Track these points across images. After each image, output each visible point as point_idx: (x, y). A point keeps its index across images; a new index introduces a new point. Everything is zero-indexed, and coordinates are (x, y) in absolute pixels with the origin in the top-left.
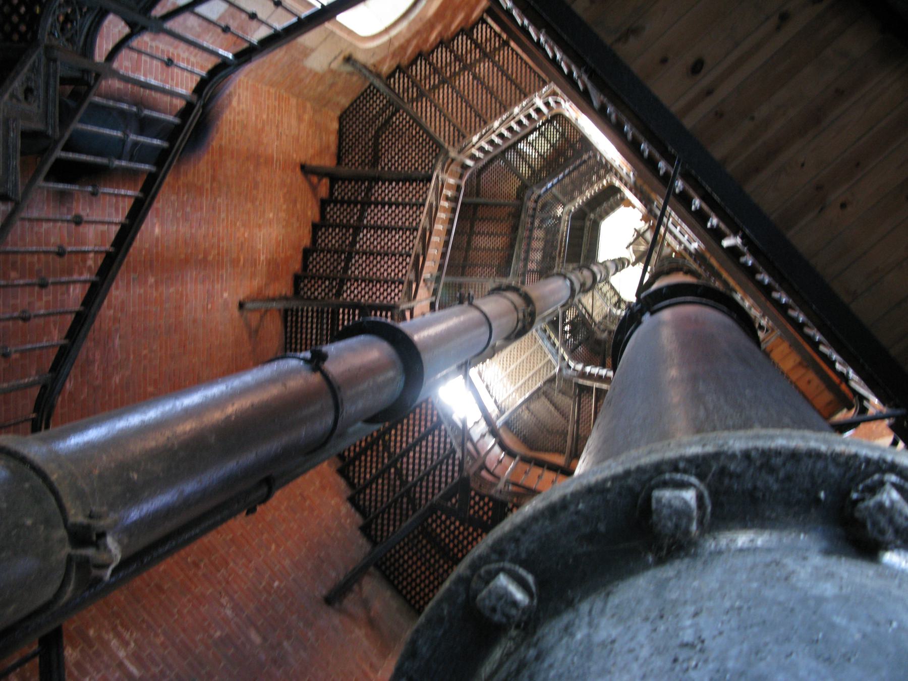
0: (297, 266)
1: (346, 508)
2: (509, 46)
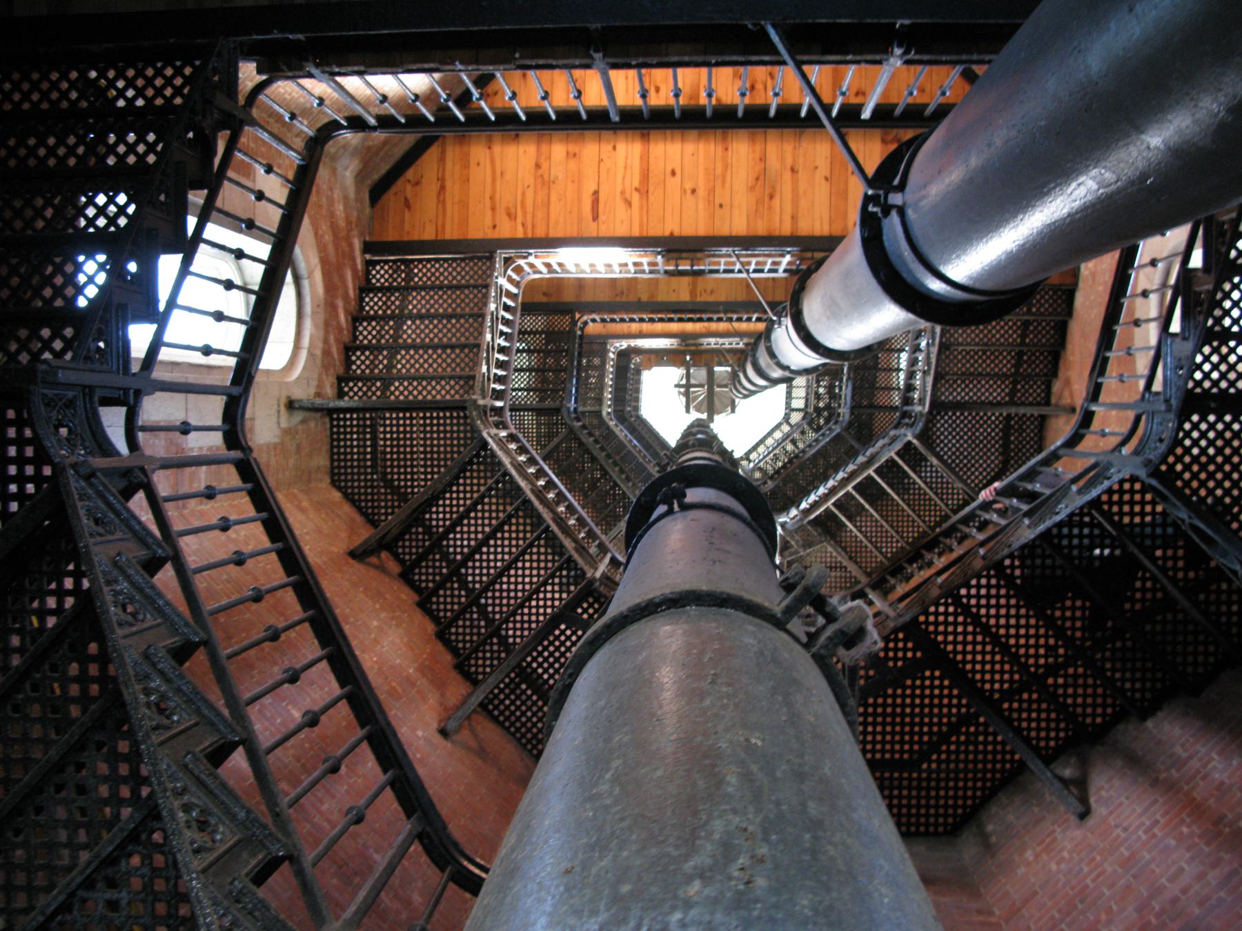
0: (448, 658)
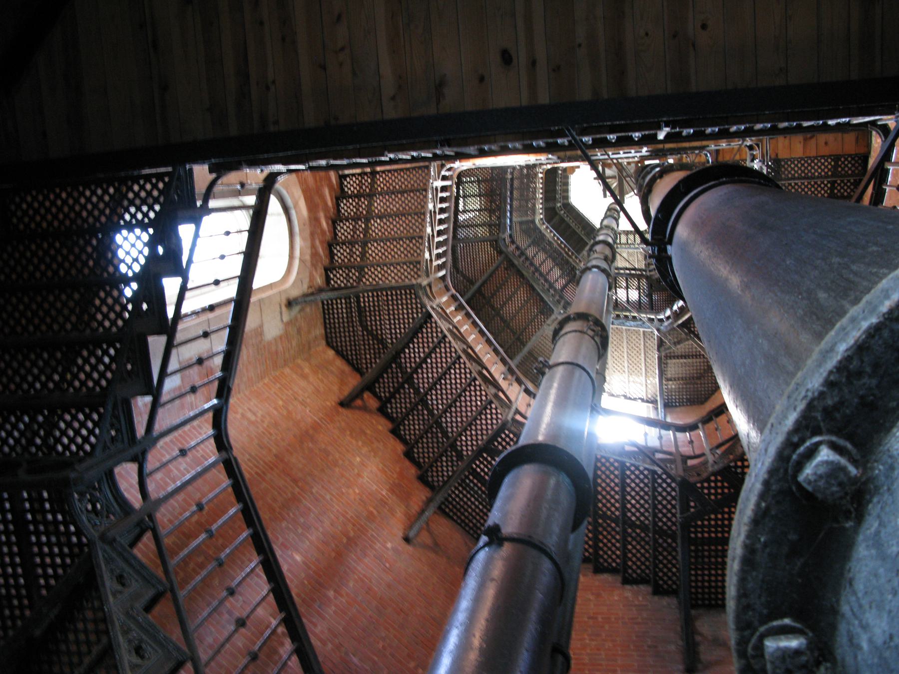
0: (413, 471)
1: (628, 592)
2: (378, 173)
